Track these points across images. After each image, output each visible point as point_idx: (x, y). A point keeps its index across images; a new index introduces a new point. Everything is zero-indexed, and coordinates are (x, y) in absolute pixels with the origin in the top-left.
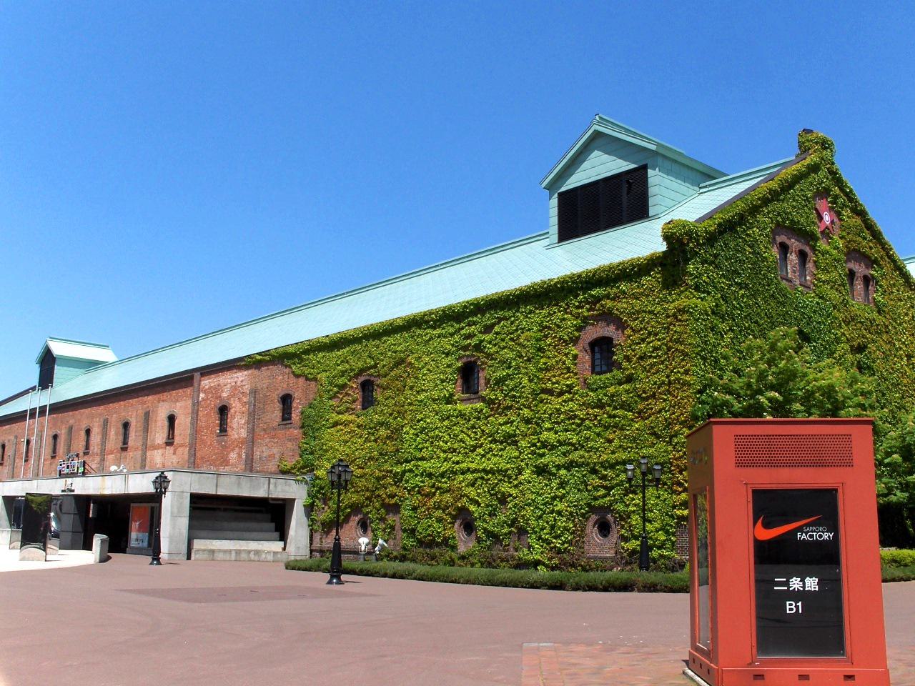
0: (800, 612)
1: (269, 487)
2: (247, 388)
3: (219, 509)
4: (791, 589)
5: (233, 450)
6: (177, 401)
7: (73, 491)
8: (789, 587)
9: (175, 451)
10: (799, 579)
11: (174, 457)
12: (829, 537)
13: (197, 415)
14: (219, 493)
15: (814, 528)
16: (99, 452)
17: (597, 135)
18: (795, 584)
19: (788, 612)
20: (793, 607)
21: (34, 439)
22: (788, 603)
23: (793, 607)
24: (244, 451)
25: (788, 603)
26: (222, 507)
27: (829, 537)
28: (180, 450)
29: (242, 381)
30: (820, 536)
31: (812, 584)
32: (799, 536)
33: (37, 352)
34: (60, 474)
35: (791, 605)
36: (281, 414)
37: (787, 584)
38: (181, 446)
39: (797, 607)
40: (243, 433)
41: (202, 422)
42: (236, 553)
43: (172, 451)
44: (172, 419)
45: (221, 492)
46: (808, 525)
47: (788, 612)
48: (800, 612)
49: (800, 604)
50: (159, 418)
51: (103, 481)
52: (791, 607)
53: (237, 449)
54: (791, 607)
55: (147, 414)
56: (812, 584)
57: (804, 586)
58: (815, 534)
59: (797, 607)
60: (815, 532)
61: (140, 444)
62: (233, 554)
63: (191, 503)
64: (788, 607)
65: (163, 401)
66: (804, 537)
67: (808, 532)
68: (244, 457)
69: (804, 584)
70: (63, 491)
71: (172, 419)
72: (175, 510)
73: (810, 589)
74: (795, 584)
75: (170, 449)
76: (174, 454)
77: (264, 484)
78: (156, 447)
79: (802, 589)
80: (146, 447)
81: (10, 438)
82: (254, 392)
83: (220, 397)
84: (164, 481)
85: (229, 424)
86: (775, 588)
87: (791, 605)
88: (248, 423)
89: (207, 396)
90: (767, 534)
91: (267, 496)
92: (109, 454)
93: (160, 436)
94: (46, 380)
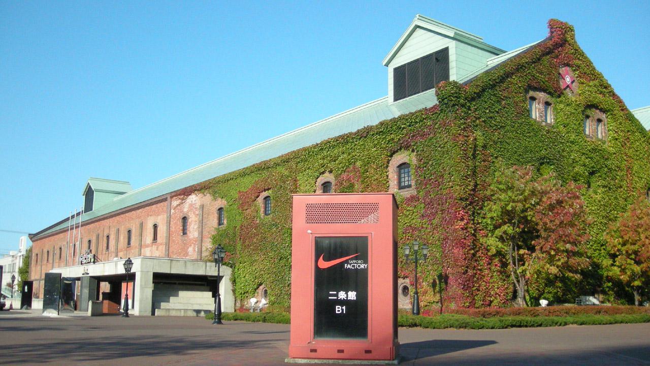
0: (344, 312)
1: (206, 268)
2: (198, 206)
3: (175, 284)
4: (339, 298)
5: (191, 246)
6: (158, 215)
7: (88, 274)
8: (338, 297)
9: (157, 248)
10: (344, 293)
11: (157, 252)
12: (365, 267)
13: (170, 224)
14: (172, 272)
15: (355, 261)
16: (114, 251)
17: (417, 27)
18: (342, 295)
19: (337, 312)
20: (340, 309)
21: (78, 244)
22: (337, 307)
23: (340, 309)
24: (196, 246)
25: (337, 307)
26: (177, 282)
27: (365, 267)
28: (160, 247)
29: (195, 201)
30: (359, 266)
31: (352, 295)
32: (346, 266)
33: (83, 188)
34: (82, 264)
35: (338, 308)
36: (218, 221)
37: (337, 295)
38: (161, 244)
39: (342, 310)
40: (196, 234)
41: (173, 229)
42: (184, 311)
43: (156, 248)
44: (155, 227)
45: (174, 271)
46: (352, 259)
47: (337, 312)
48: (344, 312)
49: (344, 308)
50: (148, 227)
51: (104, 266)
52: (339, 309)
53: (192, 245)
54: (339, 309)
55: (142, 225)
56: (352, 295)
57: (347, 297)
58: (356, 265)
59: (342, 310)
60: (356, 263)
61: (137, 245)
62: (182, 311)
63: (153, 279)
64: (337, 309)
65: (151, 216)
66: (349, 266)
67: (352, 263)
68: (196, 250)
69: (347, 295)
70: (83, 274)
71: (155, 227)
72: (143, 284)
73: (351, 298)
74: (342, 295)
75: (154, 247)
76: (157, 250)
77: (202, 266)
78: (147, 246)
79: (346, 299)
80: (141, 246)
81: (64, 243)
82: (202, 207)
83: (183, 211)
84: (129, 264)
85: (188, 229)
86: (330, 298)
87: (338, 308)
88: (199, 227)
89: (175, 211)
90: (324, 264)
91: (204, 274)
92: (120, 252)
93: (149, 238)
94: (89, 206)
